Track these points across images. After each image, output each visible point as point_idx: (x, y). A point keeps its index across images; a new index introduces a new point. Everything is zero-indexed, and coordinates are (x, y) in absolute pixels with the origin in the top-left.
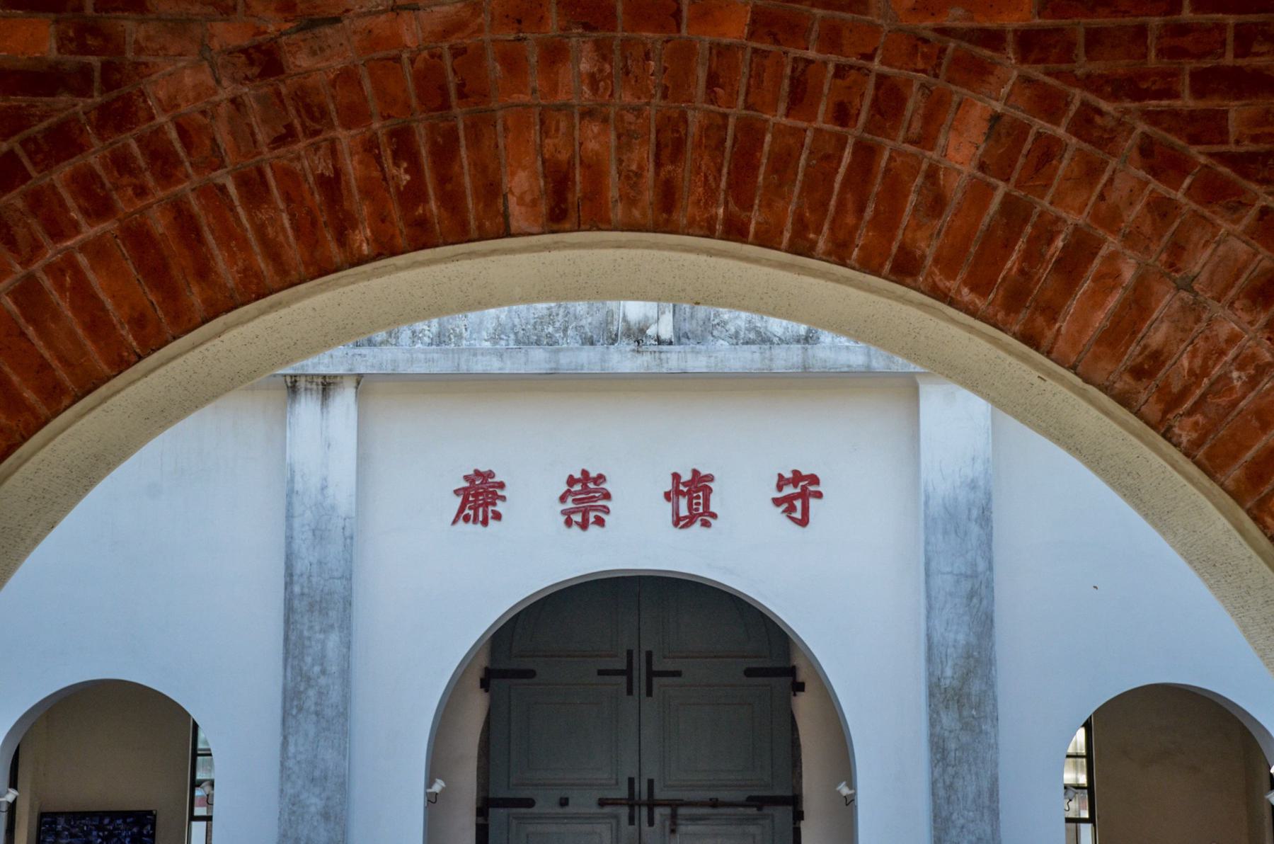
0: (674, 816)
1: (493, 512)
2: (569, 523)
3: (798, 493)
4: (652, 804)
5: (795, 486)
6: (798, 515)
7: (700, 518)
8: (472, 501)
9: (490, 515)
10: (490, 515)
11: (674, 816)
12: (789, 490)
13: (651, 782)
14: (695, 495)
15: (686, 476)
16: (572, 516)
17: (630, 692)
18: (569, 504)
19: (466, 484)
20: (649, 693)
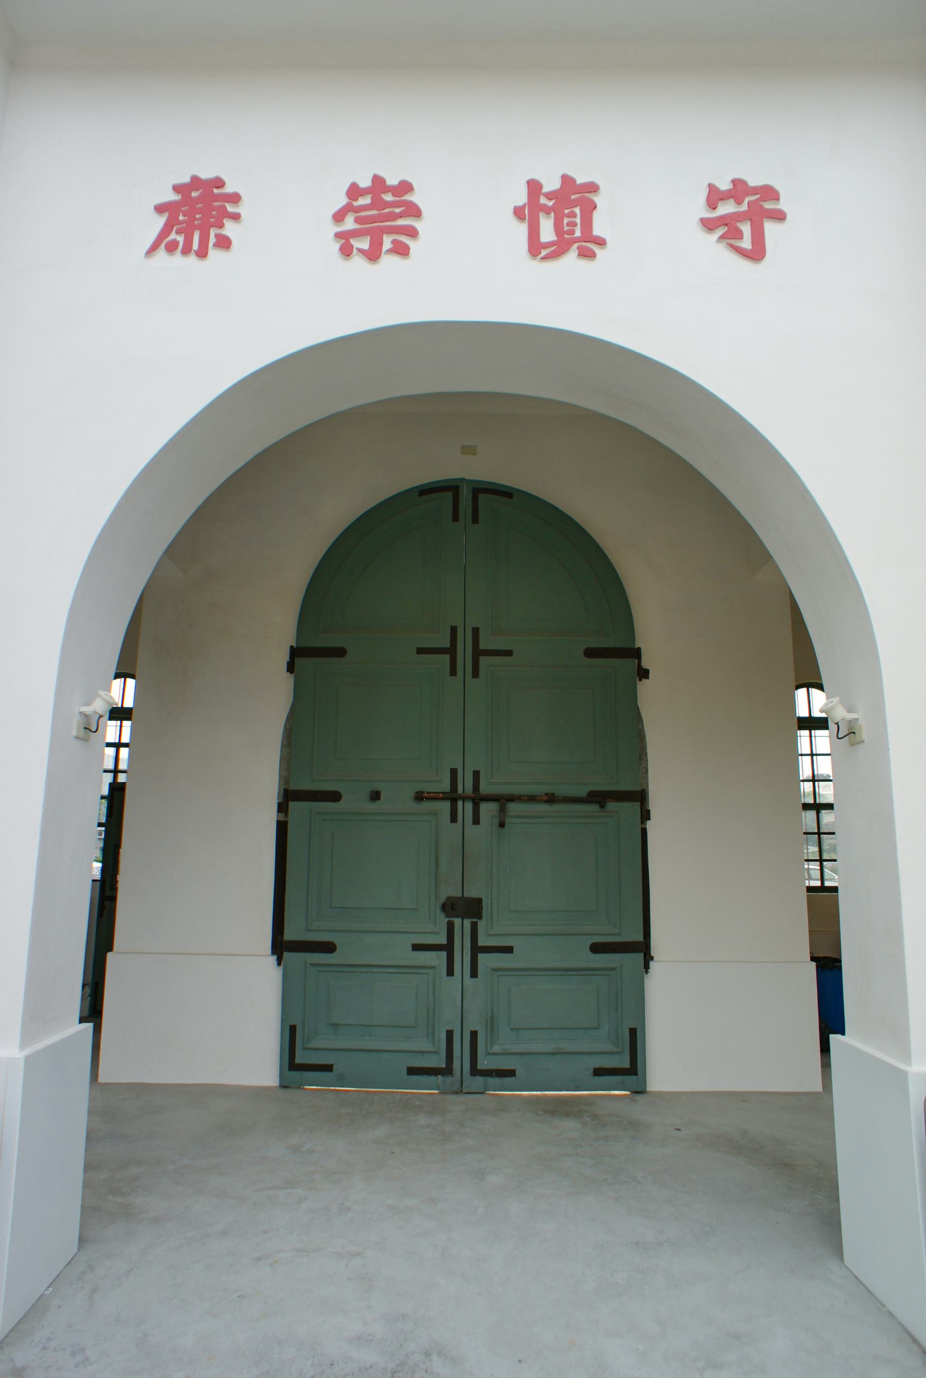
0: (502, 810)
1: (217, 236)
2: (346, 251)
3: (744, 213)
4: (477, 799)
5: (739, 202)
6: (746, 243)
7: (576, 246)
8: (183, 222)
9: (212, 240)
10: (212, 240)
11: (502, 810)
12: (726, 208)
13: (476, 774)
14: (566, 211)
15: (551, 184)
16: (352, 241)
17: (453, 672)
18: (350, 224)
19: (174, 197)
20: (476, 674)
